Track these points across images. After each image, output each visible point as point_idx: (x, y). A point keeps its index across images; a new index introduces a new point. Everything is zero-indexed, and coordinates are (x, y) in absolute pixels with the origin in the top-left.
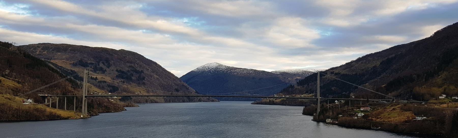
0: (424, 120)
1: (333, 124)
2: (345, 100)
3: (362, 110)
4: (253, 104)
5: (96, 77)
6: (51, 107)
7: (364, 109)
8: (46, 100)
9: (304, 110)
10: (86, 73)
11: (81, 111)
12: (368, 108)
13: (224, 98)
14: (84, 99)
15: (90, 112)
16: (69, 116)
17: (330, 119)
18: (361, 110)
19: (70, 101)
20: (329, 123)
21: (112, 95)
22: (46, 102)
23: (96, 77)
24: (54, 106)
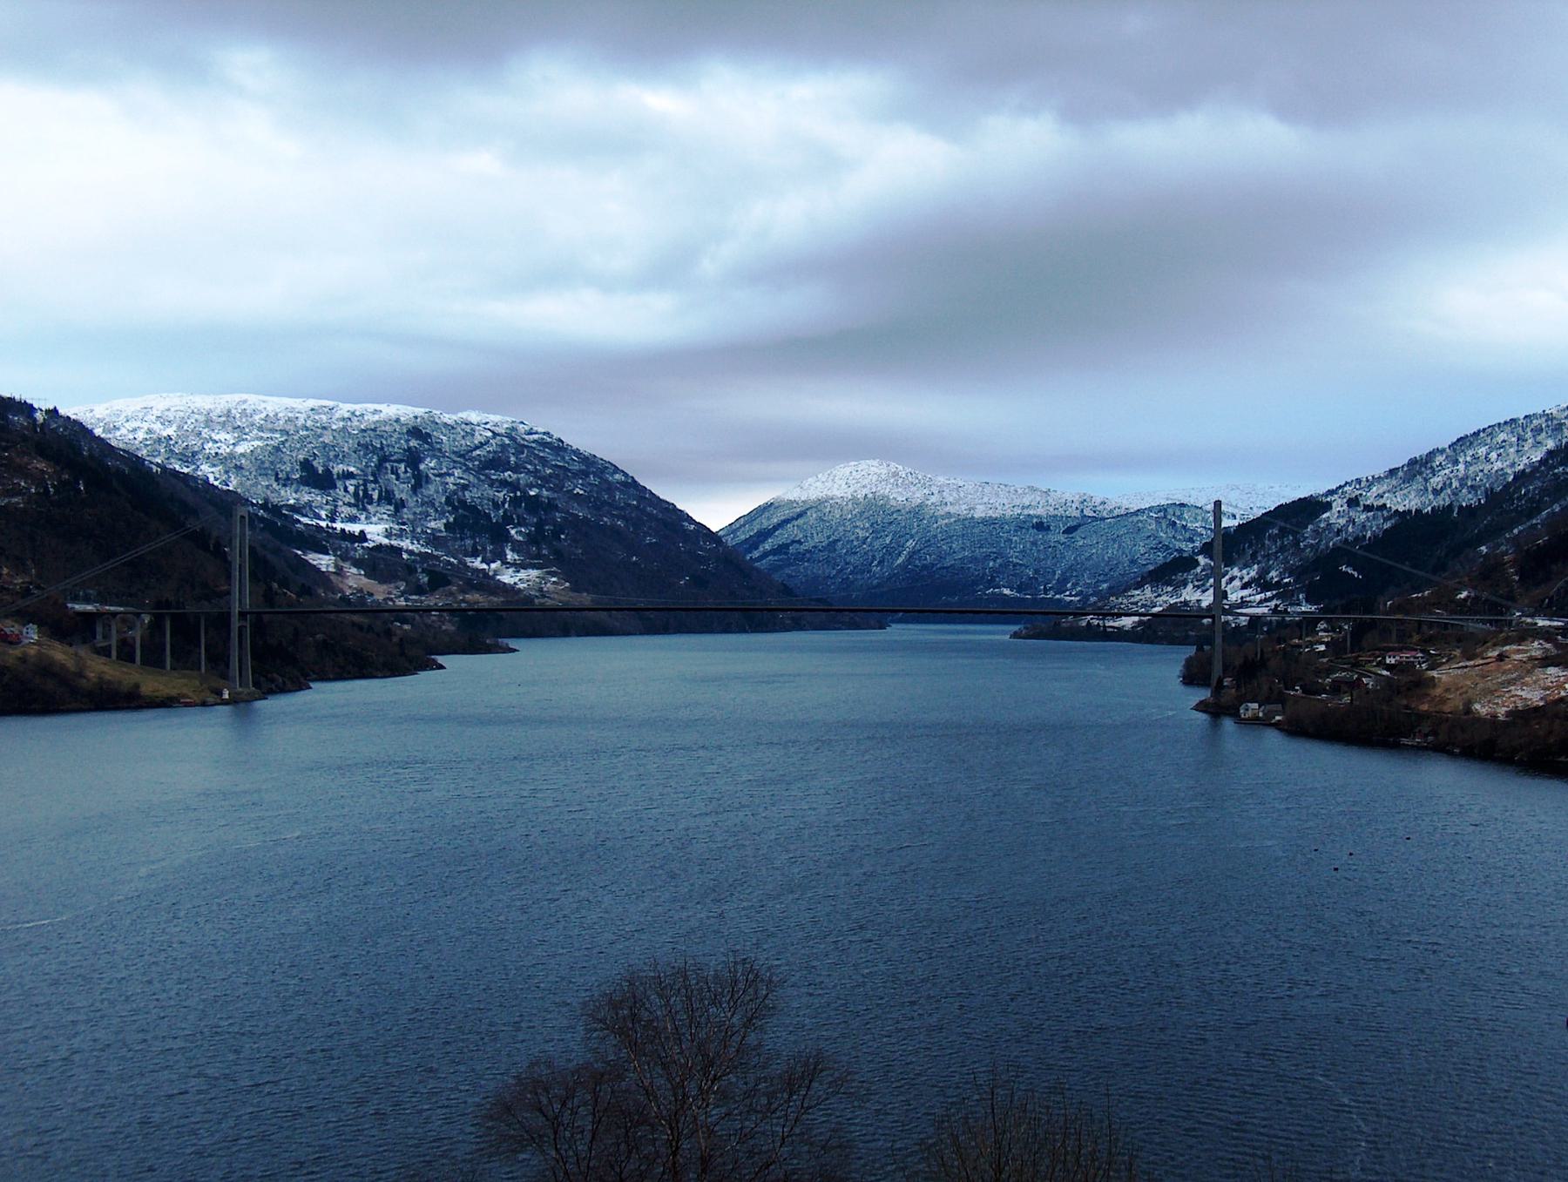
0: (1532, 616)
1: (1265, 723)
2: (1355, 619)
3: (1393, 662)
4: (1015, 635)
5: (362, 532)
6: (117, 658)
7: (1398, 658)
8: (99, 629)
9: (1189, 663)
10: (242, 517)
11: (224, 676)
12: (1414, 653)
13: (846, 617)
14: (236, 623)
15: (269, 676)
16: (174, 692)
17: (1256, 706)
18: (1388, 662)
19: (186, 631)
20: (1255, 721)
21: (785, 607)
22: (99, 637)
23: (362, 532)
24: (126, 654)
